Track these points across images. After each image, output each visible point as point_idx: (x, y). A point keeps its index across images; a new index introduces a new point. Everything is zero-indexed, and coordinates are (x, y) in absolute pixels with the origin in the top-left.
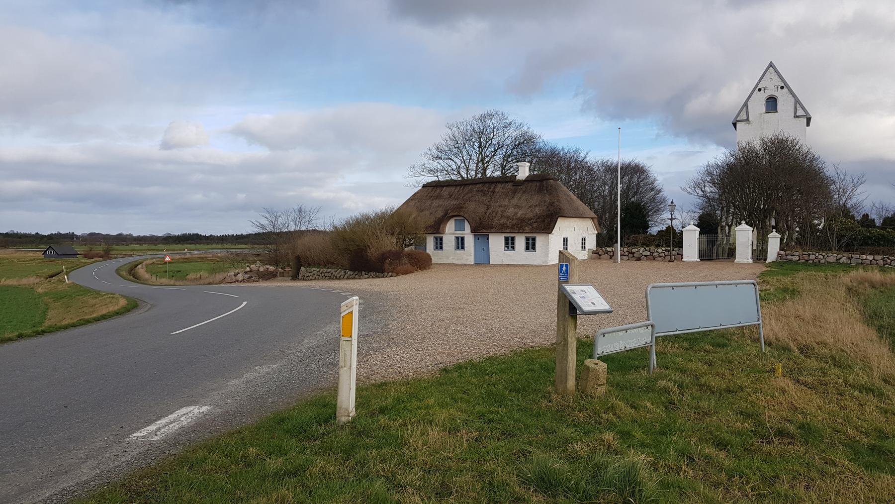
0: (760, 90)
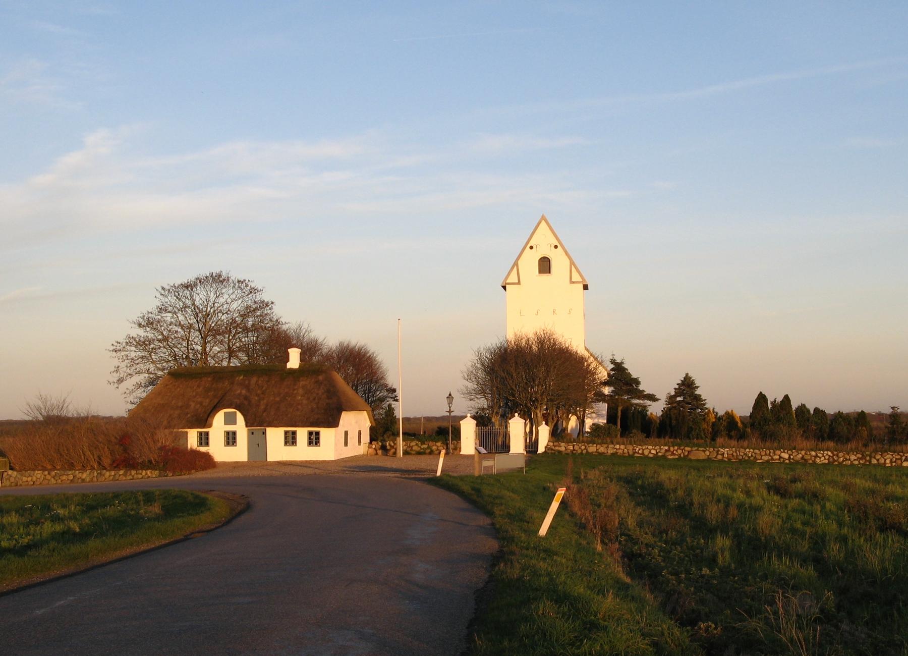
0: (531, 248)
